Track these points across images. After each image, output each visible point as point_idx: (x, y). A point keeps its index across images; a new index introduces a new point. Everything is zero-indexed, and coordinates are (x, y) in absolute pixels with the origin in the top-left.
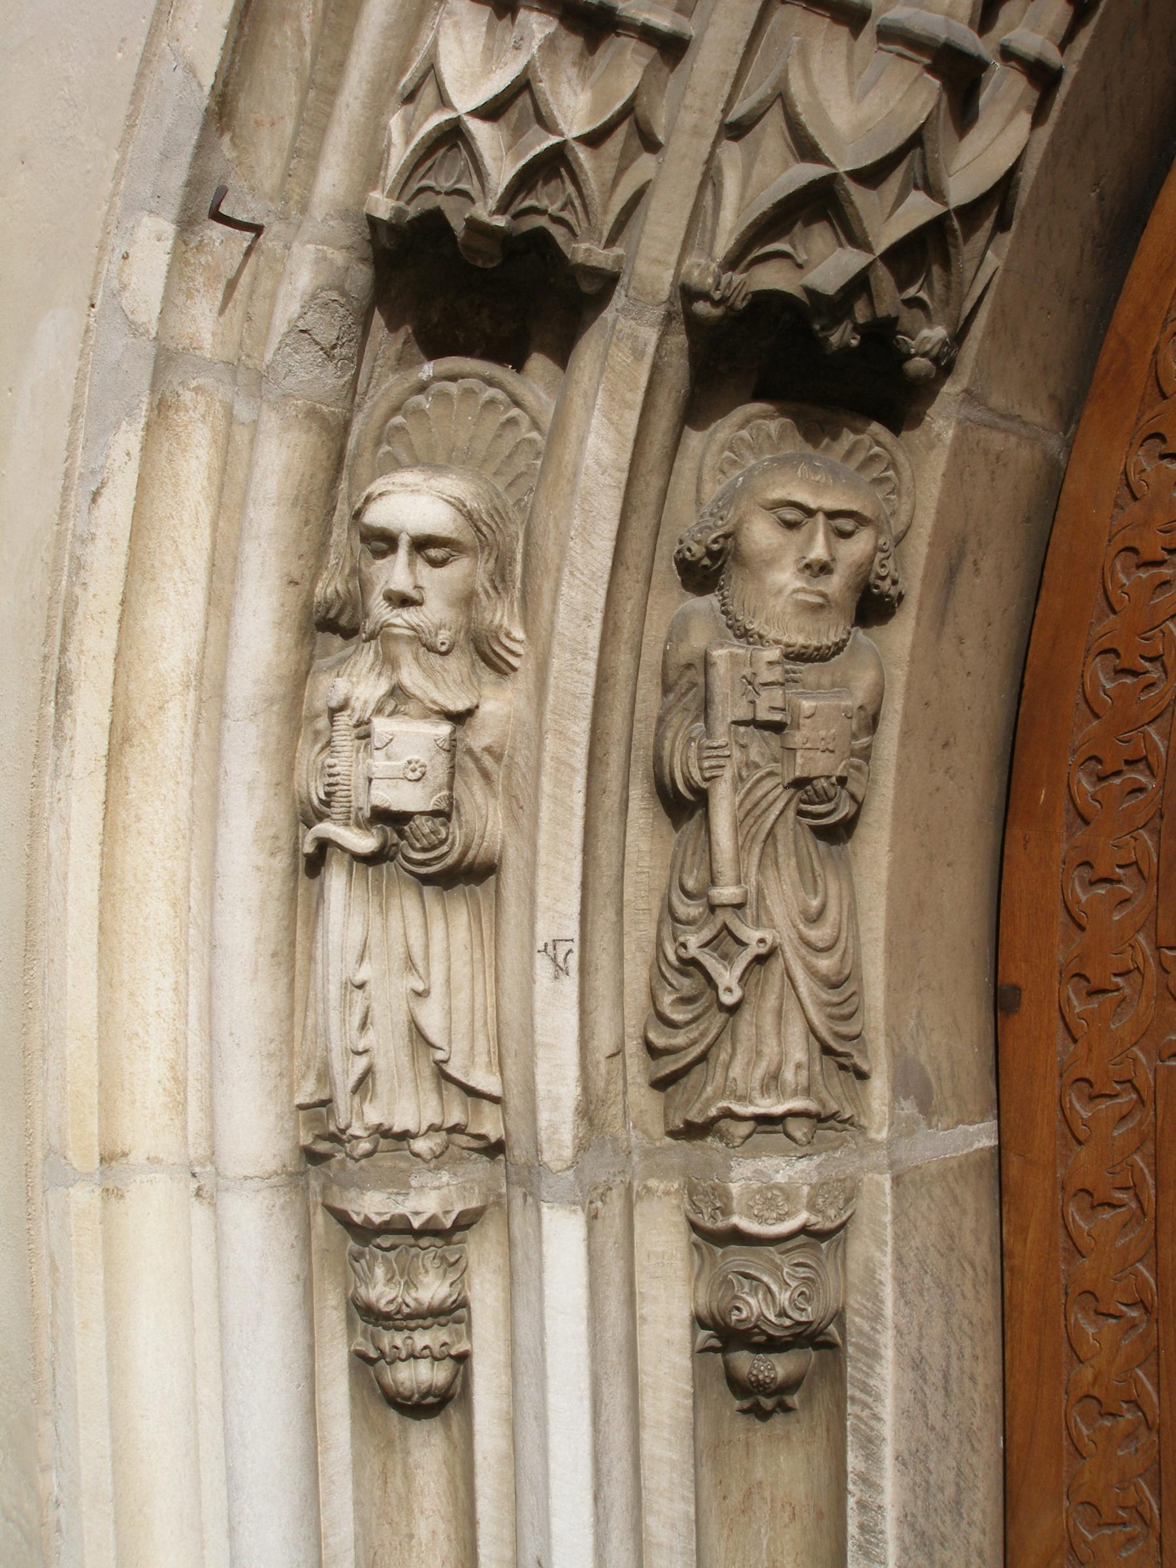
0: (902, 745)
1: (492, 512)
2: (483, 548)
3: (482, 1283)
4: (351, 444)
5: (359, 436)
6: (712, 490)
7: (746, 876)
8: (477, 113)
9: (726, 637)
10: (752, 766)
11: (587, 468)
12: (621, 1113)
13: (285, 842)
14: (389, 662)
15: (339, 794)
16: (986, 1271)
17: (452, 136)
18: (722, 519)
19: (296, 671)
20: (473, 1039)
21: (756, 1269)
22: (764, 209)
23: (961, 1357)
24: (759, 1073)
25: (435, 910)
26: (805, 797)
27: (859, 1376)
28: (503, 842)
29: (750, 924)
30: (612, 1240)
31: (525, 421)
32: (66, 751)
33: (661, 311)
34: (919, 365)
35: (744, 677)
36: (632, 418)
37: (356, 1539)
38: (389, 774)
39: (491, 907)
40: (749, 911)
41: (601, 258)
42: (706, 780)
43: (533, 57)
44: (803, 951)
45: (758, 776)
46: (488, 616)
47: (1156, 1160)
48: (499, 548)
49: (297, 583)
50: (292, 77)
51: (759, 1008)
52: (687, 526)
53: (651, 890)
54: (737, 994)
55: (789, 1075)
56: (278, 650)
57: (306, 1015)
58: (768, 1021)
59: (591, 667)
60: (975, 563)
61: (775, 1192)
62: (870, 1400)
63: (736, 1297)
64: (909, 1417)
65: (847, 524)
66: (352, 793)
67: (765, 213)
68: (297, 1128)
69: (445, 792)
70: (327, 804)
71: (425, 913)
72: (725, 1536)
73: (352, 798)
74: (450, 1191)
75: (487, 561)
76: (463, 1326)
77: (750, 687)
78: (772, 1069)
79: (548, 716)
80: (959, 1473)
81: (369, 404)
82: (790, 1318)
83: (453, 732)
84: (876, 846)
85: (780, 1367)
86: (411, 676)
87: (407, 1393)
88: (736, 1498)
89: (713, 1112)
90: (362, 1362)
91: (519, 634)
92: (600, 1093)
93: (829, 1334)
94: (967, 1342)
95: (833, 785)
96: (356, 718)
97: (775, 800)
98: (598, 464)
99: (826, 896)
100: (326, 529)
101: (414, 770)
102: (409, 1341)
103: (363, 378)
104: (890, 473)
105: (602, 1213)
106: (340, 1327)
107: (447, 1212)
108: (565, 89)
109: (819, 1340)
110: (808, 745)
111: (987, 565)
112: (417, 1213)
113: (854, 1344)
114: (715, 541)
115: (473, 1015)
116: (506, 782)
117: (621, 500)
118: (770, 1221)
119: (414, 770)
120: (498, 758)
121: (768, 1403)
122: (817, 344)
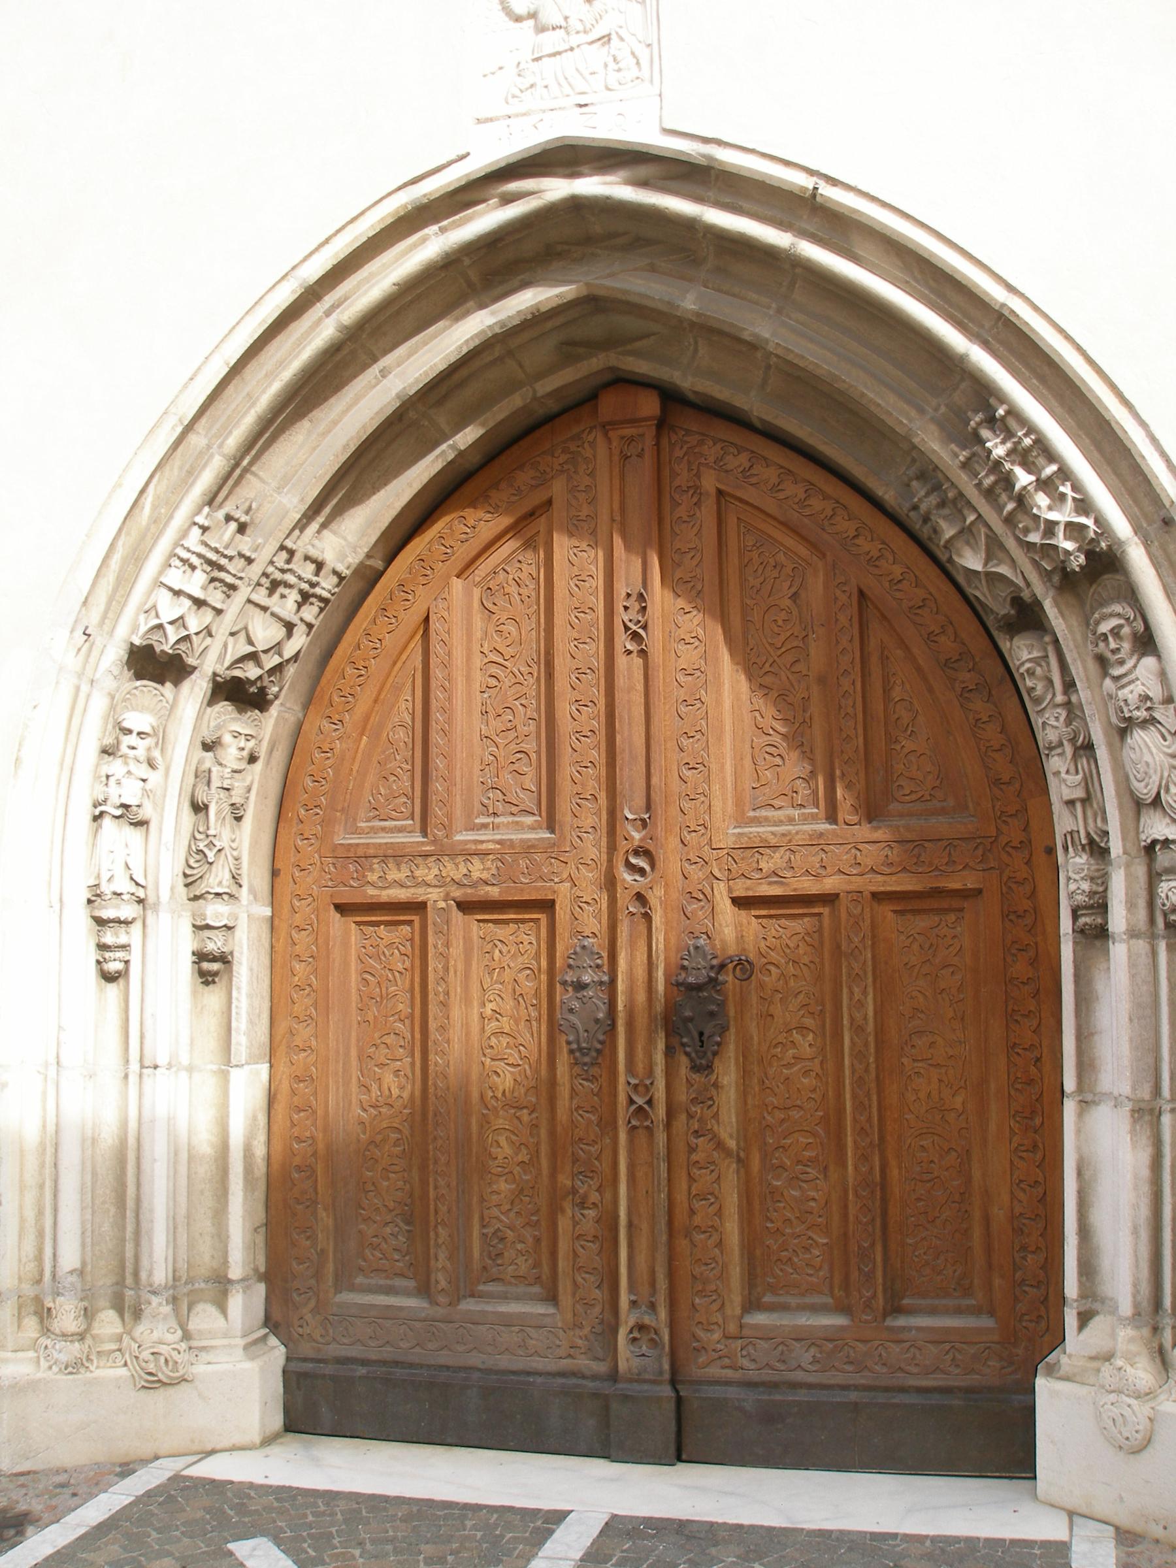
6: (213, 724)
14: (126, 763)
34: (270, 697)
47: (317, 916)
48: (159, 736)
58: (220, 867)
85: (215, 966)
109: (224, 959)
121: (210, 979)
122: (246, 691)
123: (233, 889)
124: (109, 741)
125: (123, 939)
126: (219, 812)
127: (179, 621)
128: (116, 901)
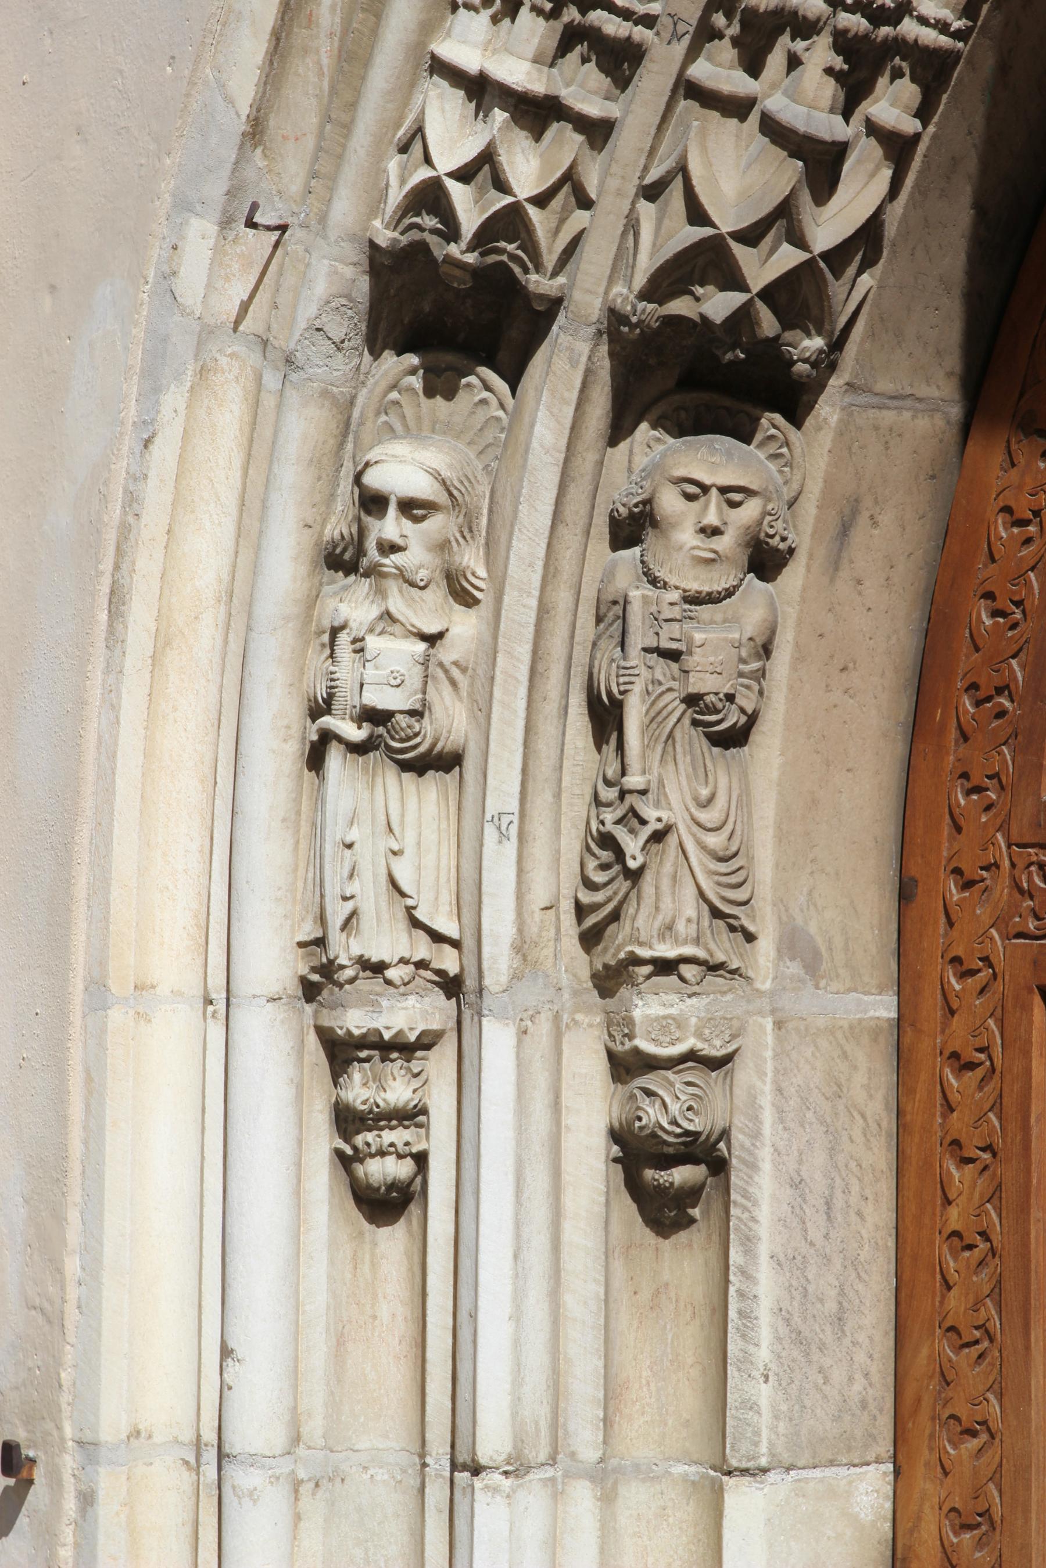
0: (794, 668)
1: (463, 479)
2: (454, 506)
4: (356, 413)
5: (363, 408)
7: (650, 768)
8: (453, 175)
9: (641, 581)
12: (552, 955)
14: (381, 593)
15: (741, 1174)
16: (879, 1125)
17: (430, 198)
18: (642, 488)
19: (308, 596)
22: (667, 257)
23: (846, 1191)
24: (657, 924)
27: (741, 1183)
28: (466, 736)
31: (494, 401)
32: (118, 651)
33: (593, 330)
36: (569, 411)
37: (328, 1308)
38: (376, 680)
41: (547, 287)
42: (622, 693)
43: (494, 137)
44: (695, 829)
45: (660, 691)
50: (314, 101)
52: (620, 491)
53: (584, 779)
55: (681, 927)
58: (665, 884)
59: (534, 603)
60: (872, 517)
61: (670, 1021)
62: (749, 1205)
63: (639, 1108)
64: (785, 1226)
65: (736, 497)
67: (668, 260)
68: (296, 960)
69: (420, 696)
71: (402, 789)
72: (635, 1326)
73: (348, 698)
76: (423, 1130)
78: (667, 921)
80: (842, 1293)
81: (372, 381)
83: (427, 650)
84: (768, 747)
85: (681, 1175)
86: (396, 604)
87: (376, 1185)
88: (645, 1295)
90: (346, 1161)
91: (482, 572)
92: (534, 936)
93: (719, 1150)
94: (854, 1181)
95: (721, 700)
96: (353, 636)
97: (673, 711)
98: (542, 446)
99: (716, 787)
100: (335, 483)
101: (395, 678)
104: (784, 450)
107: (411, 1029)
108: (519, 158)
109: (709, 1153)
110: (698, 669)
111: (887, 518)
112: (388, 1028)
113: (737, 1157)
114: (636, 505)
119: (395, 678)
120: (464, 670)
123: (722, 948)
124: (338, 525)
125: (398, 1092)
126: (654, 719)
127: (483, 168)
128: (368, 984)
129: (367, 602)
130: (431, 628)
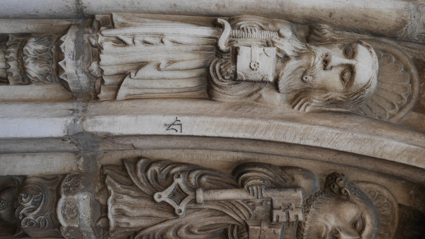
2: (347, 95)
3: (39, 90)
4: (384, 40)
10: (253, 207)
11: (383, 141)
13: (223, 11)
15: (244, 33)
18: (355, 194)
20: (140, 88)
21: (44, 205)
24: (125, 208)
25: (194, 74)
26: (240, 228)
28: (222, 102)
29: (188, 205)
30: (54, 146)
35: (291, 204)
36: (404, 161)
38: (253, 55)
39: (195, 96)
40: (192, 205)
44: (176, 226)
45: (250, 210)
46: (317, 97)
48: (349, 104)
49: (330, 17)
51: (153, 208)
54: (158, 200)
55: (124, 220)
56: (303, 8)
57: (150, 18)
58: (147, 212)
59: (297, 141)
61: (75, 214)
63: (32, 196)
66: (244, 39)
68: (103, 14)
70: (239, 29)
71: (193, 69)
74: (76, 78)
75: (341, 97)
76: (21, 82)
77: (287, 207)
78: (127, 214)
79: (276, 123)
82: (22, 219)
83: (270, 82)
86: (293, 64)
89: (109, 188)
91: (308, 109)
97: (239, 216)
99: (198, 234)
101: (255, 65)
102: (12, 59)
103: (412, 45)
105: (66, 142)
106: (19, 30)
110: (262, 231)
112: (65, 63)
114: (346, 191)
115: (150, 89)
116: (246, 103)
117: (368, 155)
118: (63, 212)
120: (256, 100)
129: (293, 49)
130: (282, 85)
